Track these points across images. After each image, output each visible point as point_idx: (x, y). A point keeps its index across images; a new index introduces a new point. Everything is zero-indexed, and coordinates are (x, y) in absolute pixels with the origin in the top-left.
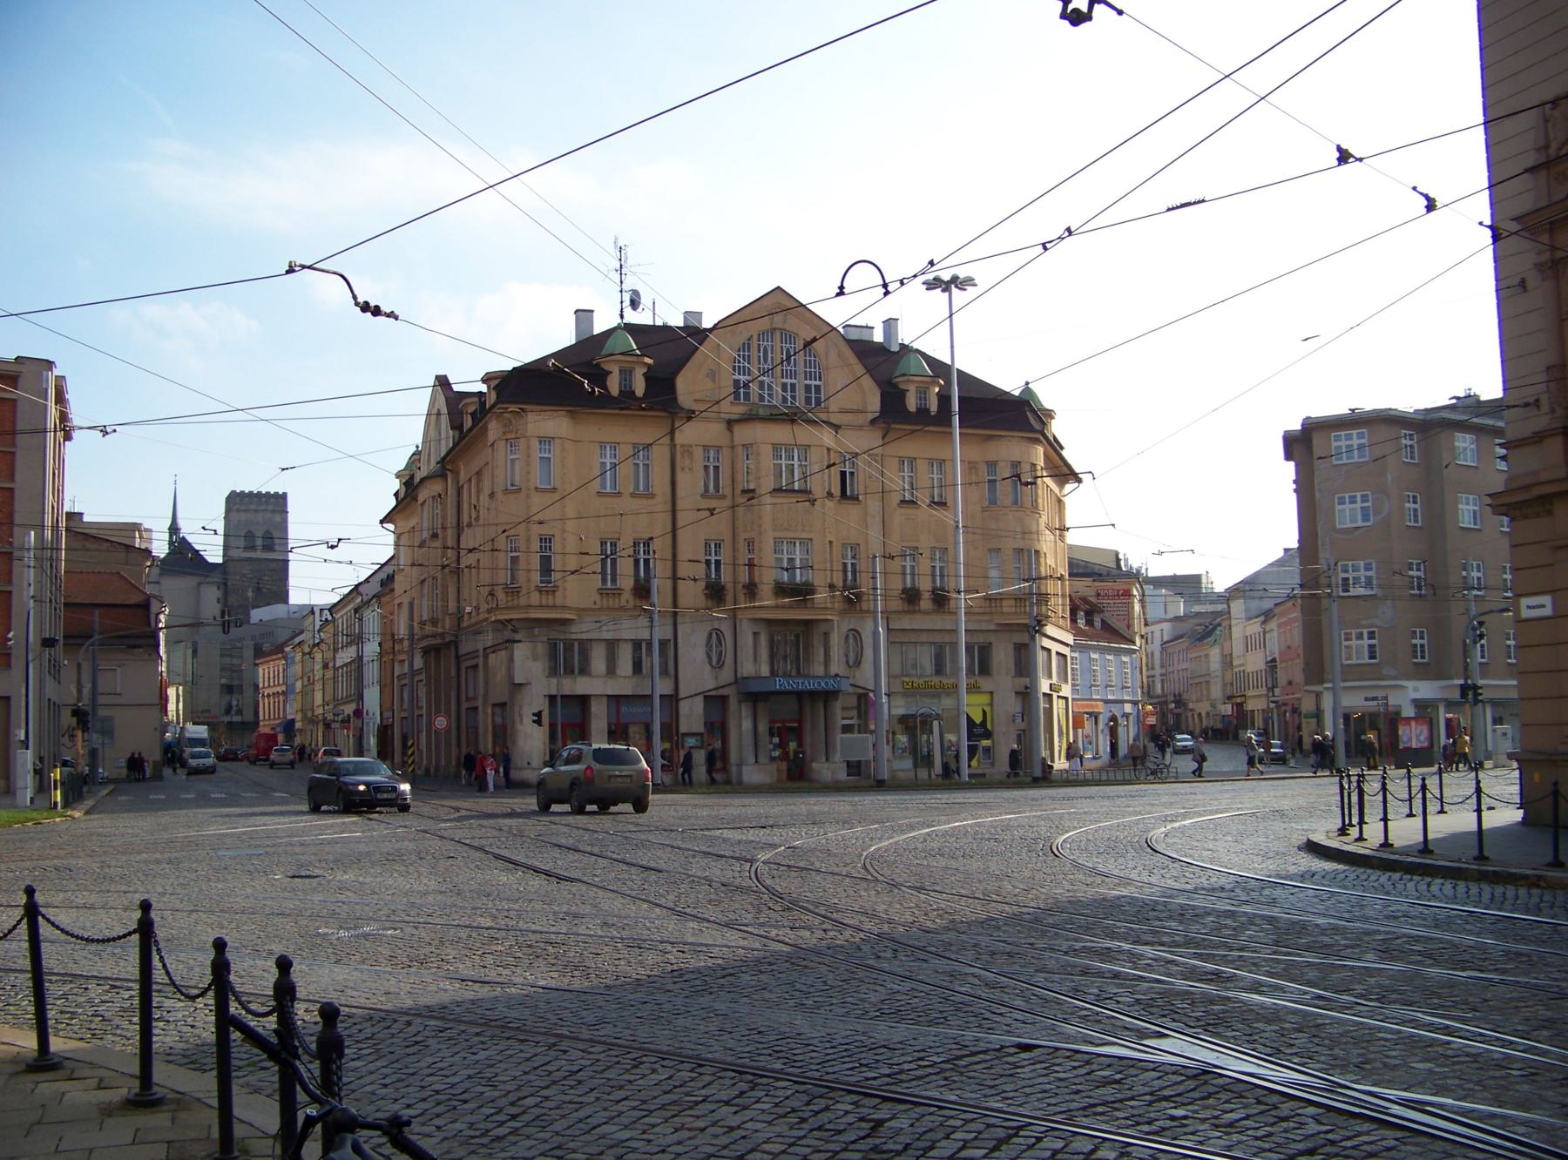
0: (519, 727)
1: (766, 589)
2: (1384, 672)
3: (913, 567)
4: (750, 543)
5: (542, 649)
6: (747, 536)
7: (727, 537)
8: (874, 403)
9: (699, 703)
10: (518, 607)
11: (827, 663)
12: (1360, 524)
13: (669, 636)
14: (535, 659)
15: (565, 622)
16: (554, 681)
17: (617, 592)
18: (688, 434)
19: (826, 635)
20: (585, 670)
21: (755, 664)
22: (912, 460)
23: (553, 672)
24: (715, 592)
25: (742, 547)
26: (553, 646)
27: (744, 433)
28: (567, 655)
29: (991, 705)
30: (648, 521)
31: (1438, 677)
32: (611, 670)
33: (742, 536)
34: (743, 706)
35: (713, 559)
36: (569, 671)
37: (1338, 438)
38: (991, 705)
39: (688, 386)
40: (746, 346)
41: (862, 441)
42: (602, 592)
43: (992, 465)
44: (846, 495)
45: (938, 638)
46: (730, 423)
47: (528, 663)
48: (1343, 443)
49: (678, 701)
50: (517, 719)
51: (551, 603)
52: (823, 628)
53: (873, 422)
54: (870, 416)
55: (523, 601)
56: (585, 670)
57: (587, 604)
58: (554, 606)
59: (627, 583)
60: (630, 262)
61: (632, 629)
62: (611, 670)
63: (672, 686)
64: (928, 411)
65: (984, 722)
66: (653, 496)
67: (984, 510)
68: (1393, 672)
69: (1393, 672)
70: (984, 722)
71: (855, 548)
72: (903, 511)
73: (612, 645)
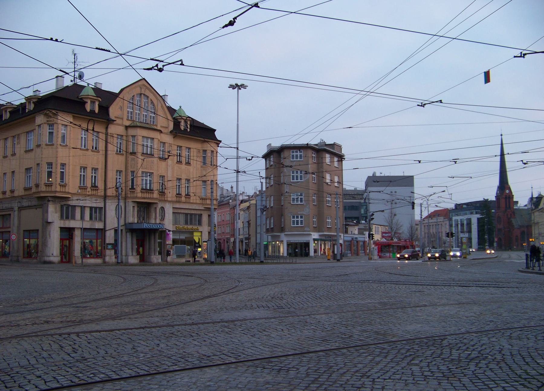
0: (49, 240)
1: (139, 189)
2: (305, 229)
3: (150, 181)
4: (133, 172)
5: (58, 208)
6: (132, 170)
7: (123, 169)
8: (171, 127)
9: (113, 232)
10: (51, 192)
11: (155, 219)
12: (299, 180)
13: (103, 206)
14: (56, 213)
15: (67, 199)
16: (62, 221)
17: (85, 188)
18: (113, 129)
19: (156, 208)
20: (73, 218)
21: (133, 218)
22: (181, 147)
23: (62, 217)
25: (130, 174)
26: (62, 207)
27: (131, 132)
28: (67, 212)
29: (201, 236)
30: (96, 160)
31: (319, 232)
32: (82, 218)
33: (130, 169)
34: (128, 234)
35: (94, 175)
36: (67, 218)
37: (293, 152)
38: (201, 236)
39: (114, 111)
41: (168, 139)
42: (80, 188)
43: (205, 151)
44: (188, 163)
45: (186, 212)
46: (127, 127)
47: (53, 213)
48: (295, 154)
49: (105, 231)
50: (48, 236)
51: (50, 190)
52: (155, 206)
53: (171, 132)
54: (170, 130)
55: (53, 189)
56: (73, 218)
57: (75, 191)
58: (65, 192)
59: (89, 184)
60: (78, 60)
61: (89, 203)
62: (82, 218)
63: (103, 225)
64: (94, 111)
65: (199, 242)
66: (98, 152)
67: (202, 167)
68: (309, 229)
69: (309, 229)
70: (199, 242)
71: (163, 177)
72: (178, 165)
73: (83, 208)
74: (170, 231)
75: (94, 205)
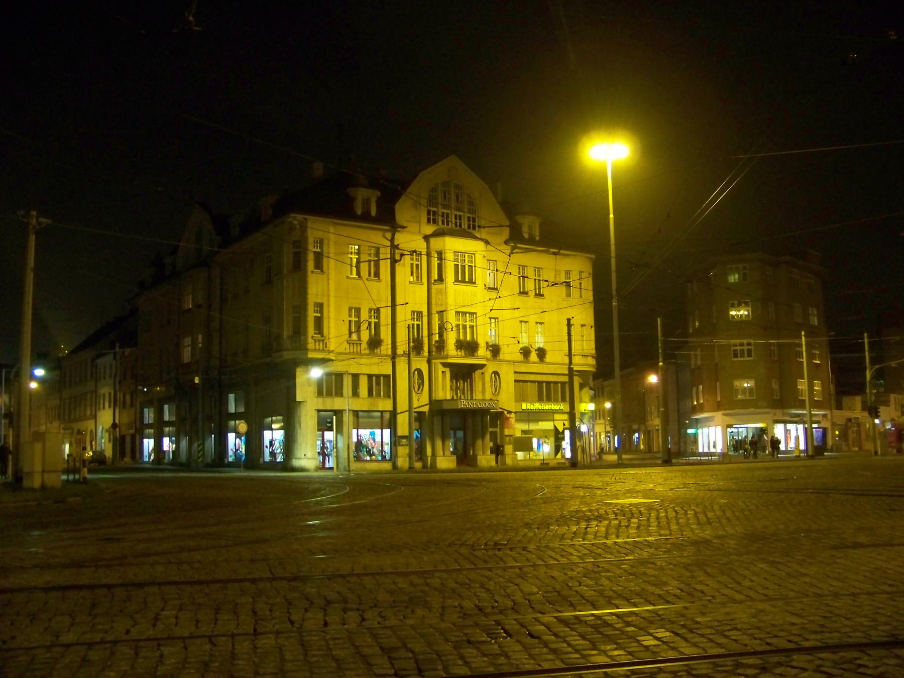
13: (390, 372)
16: (320, 400)
24: (416, 346)
32: (355, 394)
40: (434, 190)
62: (355, 394)
74: (510, 412)
75: (375, 371)
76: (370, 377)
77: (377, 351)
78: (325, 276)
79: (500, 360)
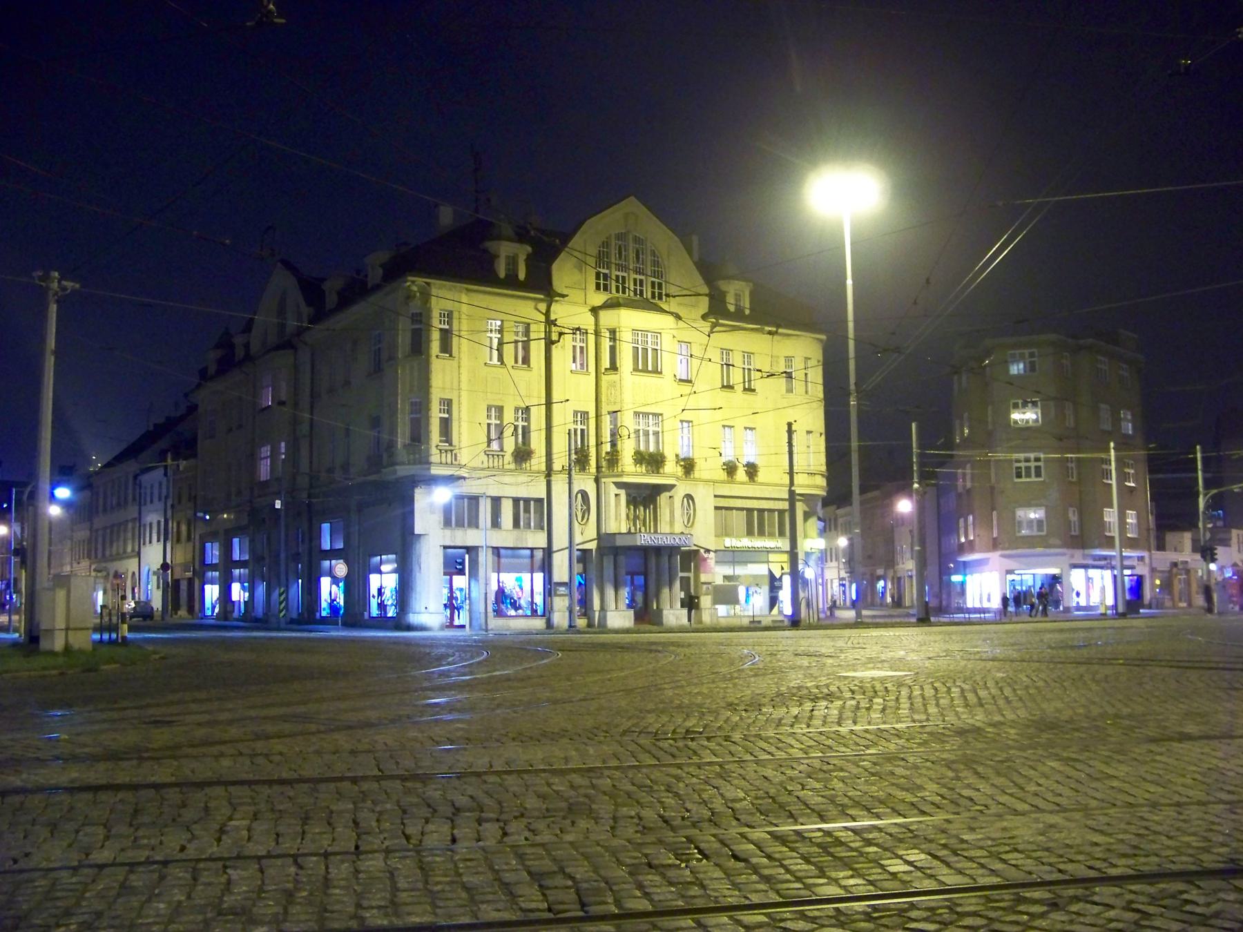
13: (544, 495)
16: (448, 532)
21: (617, 519)
24: (580, 459)
32: (496, 524)
40: (606, 244)
62: (496, 524)
74: (708, 551)
75: (523, 493)
76: (516, 501)
77: (526, 465)
78: (455, 363)
79: (695, 480)
